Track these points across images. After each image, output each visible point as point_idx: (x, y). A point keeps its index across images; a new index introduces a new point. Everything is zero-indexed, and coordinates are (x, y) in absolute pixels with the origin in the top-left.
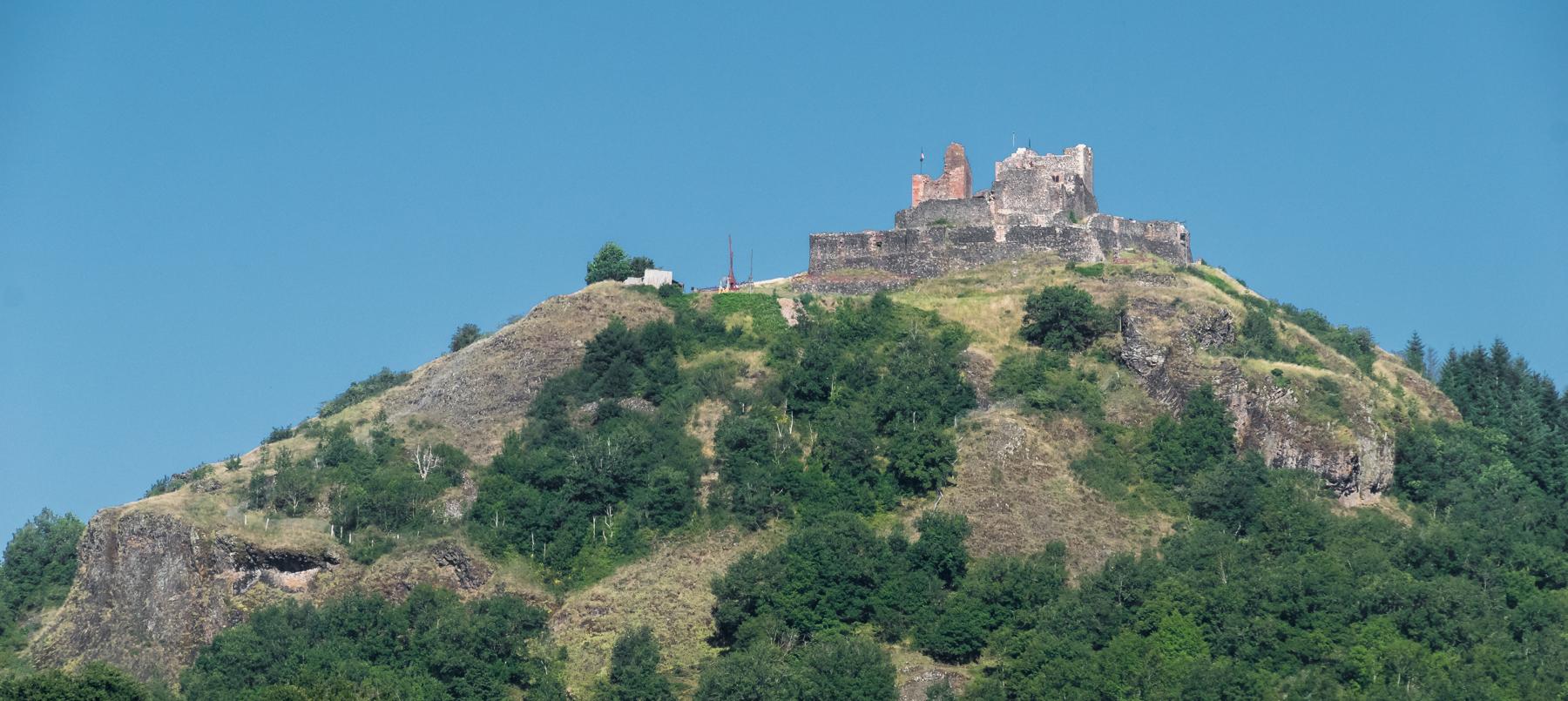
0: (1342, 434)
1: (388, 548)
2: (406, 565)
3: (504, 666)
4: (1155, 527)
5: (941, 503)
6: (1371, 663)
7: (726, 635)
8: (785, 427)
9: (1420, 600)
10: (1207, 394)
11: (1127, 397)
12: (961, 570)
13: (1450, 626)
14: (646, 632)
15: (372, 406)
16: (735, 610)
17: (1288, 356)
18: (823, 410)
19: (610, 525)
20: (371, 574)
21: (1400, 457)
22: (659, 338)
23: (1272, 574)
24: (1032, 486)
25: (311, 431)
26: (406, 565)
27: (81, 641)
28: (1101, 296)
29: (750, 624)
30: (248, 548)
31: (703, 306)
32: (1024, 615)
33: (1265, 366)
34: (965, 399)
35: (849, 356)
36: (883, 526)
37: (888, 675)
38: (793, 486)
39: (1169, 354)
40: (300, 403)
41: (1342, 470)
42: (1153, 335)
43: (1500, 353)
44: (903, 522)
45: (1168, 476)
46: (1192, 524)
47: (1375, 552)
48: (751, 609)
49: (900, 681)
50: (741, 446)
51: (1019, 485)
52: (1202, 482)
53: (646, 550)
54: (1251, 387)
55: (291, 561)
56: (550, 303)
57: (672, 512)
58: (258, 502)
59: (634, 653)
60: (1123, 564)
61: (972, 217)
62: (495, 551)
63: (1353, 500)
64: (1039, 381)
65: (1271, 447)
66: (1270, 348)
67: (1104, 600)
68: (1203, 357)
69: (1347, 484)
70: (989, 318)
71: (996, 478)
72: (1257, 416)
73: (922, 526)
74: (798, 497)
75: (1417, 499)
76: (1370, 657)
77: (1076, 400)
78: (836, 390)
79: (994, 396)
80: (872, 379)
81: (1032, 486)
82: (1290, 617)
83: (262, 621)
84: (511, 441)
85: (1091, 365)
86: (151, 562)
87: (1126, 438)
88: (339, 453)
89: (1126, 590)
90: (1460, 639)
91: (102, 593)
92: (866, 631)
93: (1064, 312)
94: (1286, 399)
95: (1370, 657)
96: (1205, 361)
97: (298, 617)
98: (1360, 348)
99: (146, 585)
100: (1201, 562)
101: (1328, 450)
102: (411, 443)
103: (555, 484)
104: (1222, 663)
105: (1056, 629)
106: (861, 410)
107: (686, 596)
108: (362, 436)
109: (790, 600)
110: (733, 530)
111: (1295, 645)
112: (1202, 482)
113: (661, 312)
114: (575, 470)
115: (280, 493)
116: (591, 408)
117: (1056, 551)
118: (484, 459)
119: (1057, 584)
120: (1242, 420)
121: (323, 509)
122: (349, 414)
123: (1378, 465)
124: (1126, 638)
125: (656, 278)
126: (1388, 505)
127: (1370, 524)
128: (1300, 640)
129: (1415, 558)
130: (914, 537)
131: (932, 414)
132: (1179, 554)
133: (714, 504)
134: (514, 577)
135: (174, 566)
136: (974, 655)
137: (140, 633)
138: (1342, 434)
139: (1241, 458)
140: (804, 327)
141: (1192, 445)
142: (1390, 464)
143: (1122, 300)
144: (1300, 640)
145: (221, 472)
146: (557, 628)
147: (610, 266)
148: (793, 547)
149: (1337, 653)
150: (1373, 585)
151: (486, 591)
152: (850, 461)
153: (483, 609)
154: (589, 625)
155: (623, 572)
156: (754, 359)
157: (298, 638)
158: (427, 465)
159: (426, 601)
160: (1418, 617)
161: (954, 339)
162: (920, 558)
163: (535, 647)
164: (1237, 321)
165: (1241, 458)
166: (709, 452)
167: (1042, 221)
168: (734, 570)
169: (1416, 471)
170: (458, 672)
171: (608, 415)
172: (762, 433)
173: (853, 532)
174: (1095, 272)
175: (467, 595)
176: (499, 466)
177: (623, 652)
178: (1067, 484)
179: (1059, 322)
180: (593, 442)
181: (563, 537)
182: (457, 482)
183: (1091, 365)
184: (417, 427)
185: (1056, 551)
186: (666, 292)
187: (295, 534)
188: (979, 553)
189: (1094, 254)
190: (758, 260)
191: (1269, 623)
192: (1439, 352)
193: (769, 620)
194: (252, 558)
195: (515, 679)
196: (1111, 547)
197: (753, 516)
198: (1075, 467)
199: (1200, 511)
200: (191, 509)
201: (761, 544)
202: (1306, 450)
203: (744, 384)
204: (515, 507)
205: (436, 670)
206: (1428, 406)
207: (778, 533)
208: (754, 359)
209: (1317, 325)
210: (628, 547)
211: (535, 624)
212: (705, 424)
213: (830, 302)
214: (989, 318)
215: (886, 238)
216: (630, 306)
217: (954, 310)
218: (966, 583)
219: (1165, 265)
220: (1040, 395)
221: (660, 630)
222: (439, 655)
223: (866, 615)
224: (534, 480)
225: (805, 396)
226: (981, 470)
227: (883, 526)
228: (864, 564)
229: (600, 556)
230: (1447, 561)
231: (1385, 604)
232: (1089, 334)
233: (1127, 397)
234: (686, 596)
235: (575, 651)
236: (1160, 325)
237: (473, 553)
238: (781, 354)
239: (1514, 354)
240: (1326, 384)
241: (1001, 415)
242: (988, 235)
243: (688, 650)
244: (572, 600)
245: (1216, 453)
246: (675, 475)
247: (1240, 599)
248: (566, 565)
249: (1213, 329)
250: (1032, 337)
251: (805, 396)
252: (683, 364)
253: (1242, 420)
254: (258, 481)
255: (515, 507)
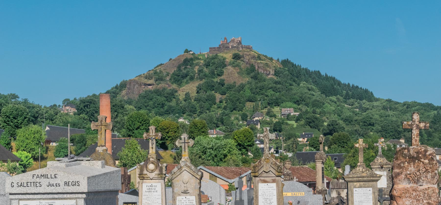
0: (268, 69)
1: (161, 83)
2: (162, 85)
3: (173, 96)
4: (247, 79)
5: (222, 77)
6: (269, 95)
7: (198, 92)
8: (205, 69)
9: (275, 87)
10: (253, 65)
11: (244, 65)
12: (224, 85)
13: (279, 90)
14: (188, 92)
15: (160, 67)
16: (198, 89)
17: (262, 60)
18: (209, 67)
19: (185, 80)
20: (159, 86)
21: (275, 71)
22: (192, 59)
23: (259, 85)
24: (233, 75)
25: (152, 70)
26: (162, 85)
27: (127, 94)
28: (241, 54)
29: (200, 91)
30: (145, 83)
31: (196, 56)
32: (231, 90)
33: (259, 61)
34: (225, 66)
35: (213, 61)
36: (215, 80)
37: (215, 97)
38: (205, 76)
39: (248, 60)
40: (152, 67)
41: (268, 73)
42: (247, 58)
43: (288, 59)
44: (217, 80)
45: (248, 74)
46: (250, 79)
47: (271, 82)
48: (200, 89)
49: (217, 97)
50: (200, 71)
51: (232, 75)
52: (252, 74)
53: (189, 83)
54: (257, 64)
55: (150, 85)
56: (177, 53)
57: (192, 79)
58: (146, 78)
59: (187, 95)
60: (242, 84)
61: (227, 45)
62: (172, 83)
63: (269, 76)
64: (234, 63)
65: (260, 71)
66: (260, 59)
67: (240, 88)
68: (252, 60)
69: (269, 74)
70: (228, 56)
71: (229, 74)
72: (258, 67)
73: (220, 80)
74: (206, 77)
75: (277, 76)
76: (269, 94)
77: (237, 65)
78: (211, 65)
79: (229, 65)
80: (215, 63)
81: (233, 75)
82: (260, 89)
83: (146, 92)
84: (175, 71)
85: (240, 62)
86: (134, 85)
87: (243, 70)
88: (156, 73)
89: (242, 87)
90: (280, 92)
91: (129, 89)
92: (213, 92)
93: (237, 56)
94: (262, 65)
95: (269, 94)
96: (253, 61)
97: (150, 91)
98: (271, 59)
99: (134, 88)
100: (251, 83)
101: (266, 71)
102: (164, 71)
103: (179, 76)
104: (252, 95)
105: (234, 91)
106: (213, 67)
107: (193, 88)
108: (158, 71)
109: (204, 88)
110: (199, 81)
111: (261, 93)
112: (252, 74)
113: (192, 56)
114: (181, 74)
115: (148, 77)
116: (184, 67)
117: (235, 82)
118: (171, 73)
119: (235, 86)
120: (257, 67)
121: (153, 79)
122: (157, 68)
123: (272, 72)
124: (242, 92)
125: (191, 53)
126: (274, 77)
127: (271, 79)
128: (262, 92)
129: (276, 83)
130: (219, 81)
131: (222, 67)
132: (249, 83)
133: (197, 78)
134: (174, 86)
135: (137, 86)
136: (225, 94)
137: (133, 93)
138: (268, 69)
139: (256, 72)
140: (208, 58)
141: (251, 71)
142: (274, 72)
143: (243, 54)
144: (262, 92)
145: (143, 75)
146: (179, 92)
147: (187, 51)
148: (205, 82)
149: (266, 93)
150: (270, 86)
151: (171, 88)
152: (213, 73)
153: (170, 90)
154: (183, 92)
155: (186, 85)
156: (202, 61)
157: (150, 93)
158: (165, 74)
159: (164, 89)
160: (275, 89)
161: (224, 59)
162: (219, 83)
163: (176, 94)
164: (257, 56)
165: (256, 72)
166: (197, 72)
167: (235, 45)
168: (199, 85)
169: (277, 73)
170: (167, 97)
171: (186, 68)
172: (202, 70)
173: (212, 81)
174: (241, 51)
175: (169, 88)
176: (173, 74)
177: (186, 94)
178: (237, 75)
179: (236, 57)
180: (183, 71)
181: (180, 82)
182: (168, 76)
183: (240, 62)
184: (164, 70)
185: (235, 82)
186: (192, 54)
187: (150, 82)
188: (226, 83)
189: (241, 49)
190: (202, 49)
191: (258, 90)
192: (280, 60)
193: (202, 91)
194: (146, 85)
195: (174, 98)
196: (241, 82)
197: (201, 79)
198: (238, 73)
199: (252, 78)
200: (139, 79)
201: (201, 82)
202: (264, 71)
203: (201, 64)
204: (174, 78)
205: (165, 97)
206: (279, 66)
207: (204, 80)
208: (202, 61)
209: (266, 56)
210: (187, 83)
211: (176, 92)
212: (196, 69)
213: (211, 55)
214: (228, 56)
215: (218, 48)
216: (189, 56)
217: (225, 55)
218: (224, 86)
219: (249, 50)
220: (234, 65)
221: (190, 92)
222: (165, 95)
223: (213, 90)
224: (177, 76)
225: (207, 65)
226: (227, 73)
227: (215, 80)
228: (213, 84)
229: (184, 84)
230: (279, 83)
231: (271, 88)
232: (240, 58)
233: (244, 65)
234: (193, 88)
235: (181, 94)
236: (247, 57)
237: (170, 84)
238: (205, 61)
239: (289, 60)
240: (266, 63)
241: (229, 67)
242: (229, 47)
243: (194, 94)
244: (181, 89)
245: (254, 71)
246: (192, 75)
247: (255, 87)
248: (180, 85)
249: (254, 57)
250: (233, 59)
251: (207, 65)
252: (194, 62)
253: (257, 67)
254: (146, 76)
255: (174, 78)
